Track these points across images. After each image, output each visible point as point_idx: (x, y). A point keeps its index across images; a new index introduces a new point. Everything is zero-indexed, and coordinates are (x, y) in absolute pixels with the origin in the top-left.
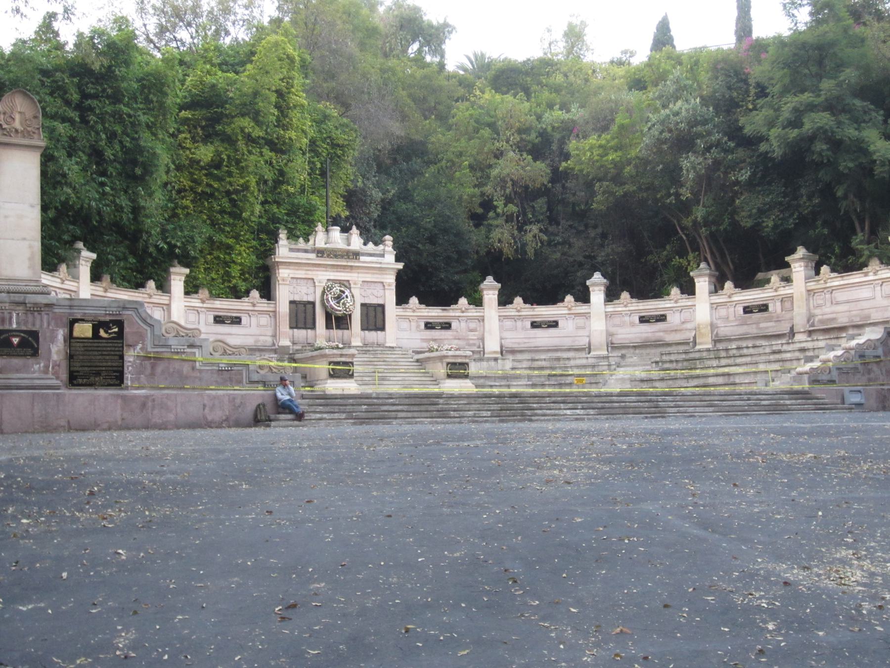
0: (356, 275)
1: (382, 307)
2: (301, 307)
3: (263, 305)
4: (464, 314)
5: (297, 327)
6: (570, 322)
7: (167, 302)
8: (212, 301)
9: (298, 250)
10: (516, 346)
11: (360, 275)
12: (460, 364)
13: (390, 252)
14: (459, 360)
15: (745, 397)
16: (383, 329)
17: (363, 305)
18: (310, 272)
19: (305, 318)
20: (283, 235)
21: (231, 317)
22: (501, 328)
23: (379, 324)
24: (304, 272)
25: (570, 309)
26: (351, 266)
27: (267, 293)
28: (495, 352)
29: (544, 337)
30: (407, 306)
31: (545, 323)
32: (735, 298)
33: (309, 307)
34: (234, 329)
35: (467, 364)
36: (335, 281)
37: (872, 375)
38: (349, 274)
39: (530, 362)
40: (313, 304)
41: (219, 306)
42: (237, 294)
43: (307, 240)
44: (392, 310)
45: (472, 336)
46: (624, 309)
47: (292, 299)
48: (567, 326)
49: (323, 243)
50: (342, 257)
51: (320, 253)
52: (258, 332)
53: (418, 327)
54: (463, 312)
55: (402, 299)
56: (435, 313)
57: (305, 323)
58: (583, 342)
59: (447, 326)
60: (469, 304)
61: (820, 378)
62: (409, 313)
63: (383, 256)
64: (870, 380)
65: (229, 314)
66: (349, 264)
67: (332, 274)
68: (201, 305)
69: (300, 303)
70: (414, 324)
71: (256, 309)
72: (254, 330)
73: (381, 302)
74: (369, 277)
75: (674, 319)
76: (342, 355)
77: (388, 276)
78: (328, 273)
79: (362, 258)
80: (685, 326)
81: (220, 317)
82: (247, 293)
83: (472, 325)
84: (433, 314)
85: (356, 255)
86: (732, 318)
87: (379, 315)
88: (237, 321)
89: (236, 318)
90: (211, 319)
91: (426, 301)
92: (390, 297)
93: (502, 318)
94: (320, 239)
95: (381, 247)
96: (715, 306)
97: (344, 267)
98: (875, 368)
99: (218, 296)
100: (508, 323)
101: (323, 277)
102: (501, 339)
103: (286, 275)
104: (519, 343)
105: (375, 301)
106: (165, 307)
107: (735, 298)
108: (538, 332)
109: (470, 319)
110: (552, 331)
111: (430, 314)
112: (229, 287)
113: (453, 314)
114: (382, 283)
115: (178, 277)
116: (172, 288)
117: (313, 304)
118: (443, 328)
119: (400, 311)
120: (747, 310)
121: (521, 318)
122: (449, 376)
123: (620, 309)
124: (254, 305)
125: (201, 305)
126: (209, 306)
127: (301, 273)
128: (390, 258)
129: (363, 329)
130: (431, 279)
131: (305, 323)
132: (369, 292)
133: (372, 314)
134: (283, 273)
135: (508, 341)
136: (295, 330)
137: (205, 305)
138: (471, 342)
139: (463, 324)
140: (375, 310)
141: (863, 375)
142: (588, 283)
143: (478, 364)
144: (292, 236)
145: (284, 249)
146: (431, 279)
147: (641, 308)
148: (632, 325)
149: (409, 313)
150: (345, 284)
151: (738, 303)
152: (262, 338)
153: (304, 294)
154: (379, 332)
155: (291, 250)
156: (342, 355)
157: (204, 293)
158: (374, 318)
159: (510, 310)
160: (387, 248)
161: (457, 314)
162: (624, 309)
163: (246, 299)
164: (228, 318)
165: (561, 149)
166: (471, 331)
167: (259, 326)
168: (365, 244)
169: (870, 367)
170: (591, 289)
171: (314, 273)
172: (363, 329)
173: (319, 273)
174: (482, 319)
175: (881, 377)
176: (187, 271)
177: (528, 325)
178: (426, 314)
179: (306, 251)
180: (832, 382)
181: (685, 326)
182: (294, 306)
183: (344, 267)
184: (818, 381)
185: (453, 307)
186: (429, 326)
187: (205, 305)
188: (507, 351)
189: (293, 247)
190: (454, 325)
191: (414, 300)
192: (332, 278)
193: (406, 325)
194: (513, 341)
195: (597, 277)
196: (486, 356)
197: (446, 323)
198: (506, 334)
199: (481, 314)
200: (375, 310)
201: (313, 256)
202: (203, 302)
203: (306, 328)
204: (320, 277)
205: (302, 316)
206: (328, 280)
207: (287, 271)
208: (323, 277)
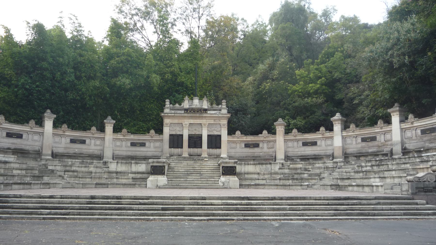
1: (220, 136)
4: (266, 139)
7: (103, 137)
13: (224, 108)
16: (220, 148)
18: (180, 120)
20: (167, 102)
24: (177, 120)
27: (160, 131)
30: (234, 136)
31: (310, 143)
32: (416, 124)
38: (201, 120)
41: (133, 138)
43: (180, 105)
44: (225, 137)
47: (171, 133)
48: (322, 144)
51: (186, 110)
54: (265, 138)
55: (231, 132)
56: (250, 139)
57: (178, 145)
58: (329, 152)
62: (61, 132)
63: (220, 110)
67: (192, 120)
68: (123, 137)
71: (153, 139)
72: (152, 149)
73: (181, 133)
74: (212, 122)
75: (381, 139)
77: (223, 121)
78: (190, 120)
79: (209, 112)
80: (387, 143)
81: (134, 143)
84: (249, 139)
86: (414, 138)
91: (245, 132)
92: (224, 133)
93: (286, 141)
94: (186, 104)
95: (220, 106)
96: (404, 130)
100: (118, 143)
102: (113, 151)
103: (168, 122)
105: (216, 133)
107: (416, 124)
109: (35, 133)
111: (247, 139)
116: (106, 130)
119: (231, 138)
120: (424, 132)
121: (298, 141)
123: (350, 134)
125: (123, 137)
127: (176, 121)
128: (225, 111)
129: (170, 147)
131: (178, 145)
134: (166, 121)
137: (125, 138)
151: (417, 127)
154: (218, 149)
156: (158, 162)
158: (215, 142)
161: (262, 139)
162: (352, 134)
165: (215, 20)
167: (95, 145)
170: (334, 123)
171: (182, 120)
173: (185, 120)
174: (275, 141)
178: (245, 139)
181: (387, 143)
188: (116, 158)
195: (338, 116)
197: (256, 144)
199: (275, 139)
201: (183, 112)
202: (124, 136)
203: (178, 147)
207: (169, 120)
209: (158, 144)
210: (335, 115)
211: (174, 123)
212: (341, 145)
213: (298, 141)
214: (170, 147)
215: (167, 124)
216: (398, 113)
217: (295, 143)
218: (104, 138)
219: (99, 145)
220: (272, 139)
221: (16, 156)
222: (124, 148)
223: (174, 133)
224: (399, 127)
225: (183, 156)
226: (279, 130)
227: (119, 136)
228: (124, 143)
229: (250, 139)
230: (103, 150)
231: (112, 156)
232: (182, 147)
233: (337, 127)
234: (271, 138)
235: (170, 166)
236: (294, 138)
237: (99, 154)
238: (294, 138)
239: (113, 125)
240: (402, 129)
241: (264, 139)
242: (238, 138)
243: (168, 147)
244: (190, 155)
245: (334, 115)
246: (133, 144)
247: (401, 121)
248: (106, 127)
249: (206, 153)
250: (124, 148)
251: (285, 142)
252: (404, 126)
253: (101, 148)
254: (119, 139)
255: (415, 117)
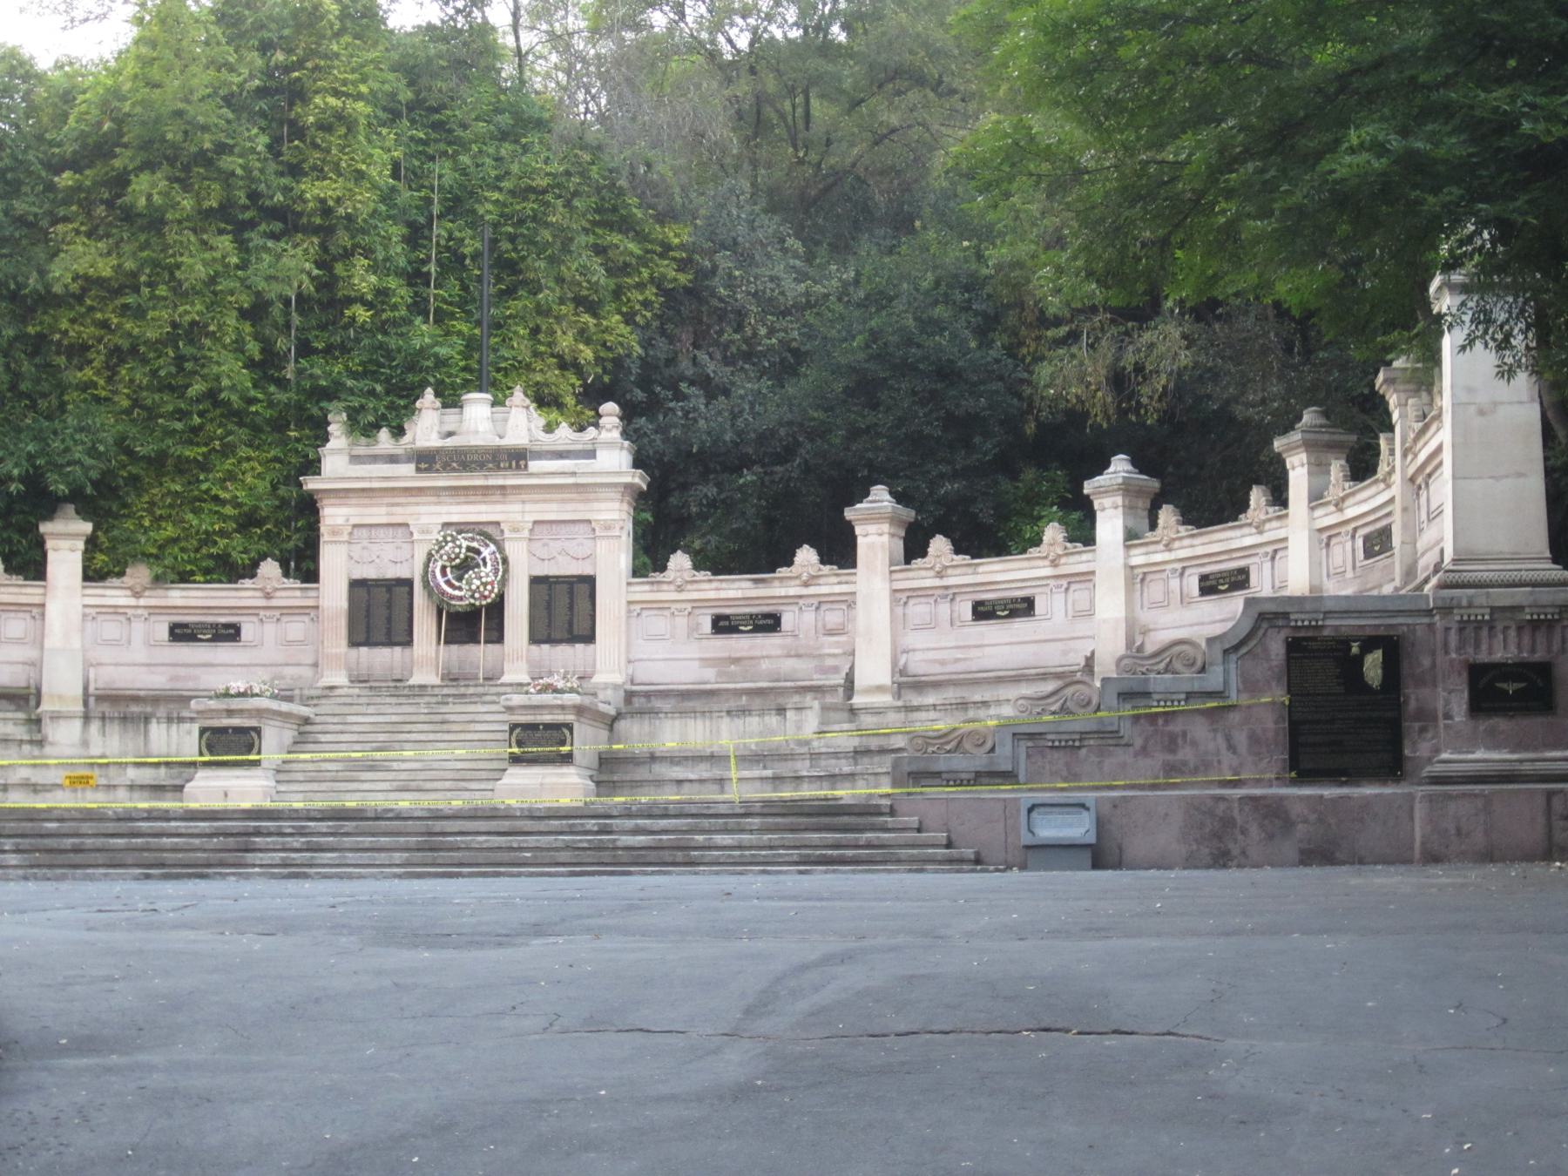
0: (517, 507)
2: (381, 595)
3: (291, 592)
4: (812, 590)
5: (368, 643)
6: (270, 629)
7: (37, 600)
8: (160, 592)
9: (375, 459)
10: (937, 669)
11: (528, 507)
12: (549, 727)
13: (610, 445)
14: (547, 718)
15: (591, 824)
16: (589, 638)
17: (536, 581)
18: (399, 510)
19: (389, 619)
21: (215, 626)
22: (898, 624)
23: (580, 628)
24: (383, 510)
25: (1054, 563)
26: (503, 487)
27: (303, 565)
28: (880, 689)
29: (1003, 645)
30: (658, 577)
33: (583, 588)
34: (223, 653)
35: (258, 731)
36: (462, 527)
37: (1185, 754)
38: (499, 507)
39: (902, 716)
40: (408, 583)
41: (179, 602)
42: (232, 571)
43: (399, 432)
45: (831, 646)
46: (1167, 556)
47: (357, 575)
49: (435, 436)
50: (481, 466)
51: (426, 460)
52: (280, 659)
53: (693, 629)
54: (806, 584)
55: (651, 553)
56: (737, 591)
57: (389, 632)
59: (769, 623)
60: (823, 562)
61: (941, 766)
62: (669, 595)
64: (1171, 769)
65: (210, 619)
66: (491, 482)
68: (133, 602)
69: (379, 583)
70: (682, 621)
71: (274, 603)
74: (551, 511)
76: (230, 713)
77: (603, 506)
78: (444, 509)
79: (534, 465)
82: (250, 571)
83: (833, 618)
84: (732, 594)
85: (517, 458)
87: (581, 604)
88: (229, 633)
89: (227, 626)
90: (164, 632)
91: (715, 563)
92: (611, 559)
93: (902, 598)
94: (428, 425)
97: (486, 490)
98: (1200, 730)
99: (184, 578)
100: (111, 628)
101: (430, 517)
103: (340, 521)
104: (943, 663)
106: (35, 611)
108: (991, 631)
109: (821, 603)
110: (1020, 626)
111: (723, 595)
112: (211, 556)
113: (782, 592)
114: (589, 521)
115: (65, 544)
117: (408, 583)
118: (758, 629)
121: (950, 593)
122: (516, 760)
124: (268, 596)
125: (133, 602)
126: (153, 602)
127: (378, 513)
129: (354, 643)
130: (734, 503)
131: (389, 632)
132: (555, 546)
133: (562, 601)
134: (333, 516)
135: (918, 656)
136: (364, 650)
137: (142, 602)
138: (830, 662)
139: (809, 617)
140: (571, 593)
141: (1144, 751)
142: (1088, 487)
143: (739, 722)
144: (362, 428)
145: (338, 459)
146: (734, 503)
147: (1200, 551)
148: (1184, 600)
149: (669, 595)
150: (487, 532)
152: (289, 671)
153: (386, 562)
154: (579, 647)
155: (356, 459)
156: (230, 713)
157: (139, 574)
158: (565, 609)
159: (921, 575)
160: (605, 436)
161: (792, 591)
162: (1167, 556)
163: (247, 583)
164: (204, 627)
166: (830, 633)
168: (549, 428)
169: (1176, 727)
172: (535, 639)
173: (422, 509)
174: (849, 601)
175: (1227, 758)
176: (87, 527)
177: (966, 610)
178: (712, 595)
179: (393, 459)
180: (1009, 776)
182: (362, 592)
183: (486, 490)
184: (938, 774)
185: (783, 572)
186: (723, 625)
187: (142, 602)
189: (361, 451)
190: (787, 621)
191: (680, 562)
192: (455, 519)
193: (654, 629)
194: (931, 655)
196: (857, 700)
198: (913, 639)
200: (571, 593)
202: (137, 595)
203: (390, 643)
204: (424, 520)
205: (379, 612)
206: (446, 525)
207: (344, 511)
208: (430, 517)
209: (296, 628)
210: (1107, 465)
211: (371, 526)
212: (1120, 613)
213: (950, 593)
214: (354, 643)
215: (335, 532)
216: (1119, 500)
217: (944, 608)
218: (43, 605)
219: (19, 641)
220: (837, 589)
221: (489, 396)
222: (139, 654)
223: (370, 573)
224: (1121, 561)
225: (416, 680)
226: (871, 546)
227: (113, 595)
228: (138, 628)
229: (739, 594)
230: (36, 665)
231: (80, 691)
232: (408, 642)
233: (1110, 523)
234: (832, 582)
235: (1485, 632)
236: (938, 582)
237: (23, 684)
238: (938, 582)
239: (81, 545)
240: (1132, 568)
241: (805, 591)
242: (680, 589)
243: (344, 642)
244: (451, 678)
245: (1101, 466)
246: (182, 633)
247: (1131, 536)
248: (51, 556)
249: (523, 665)
250: (139, 654)
251: (894, 602)
252: (1138, 558)
253: (30, 653)
254: (116, 610)
255: (1186, 521)
